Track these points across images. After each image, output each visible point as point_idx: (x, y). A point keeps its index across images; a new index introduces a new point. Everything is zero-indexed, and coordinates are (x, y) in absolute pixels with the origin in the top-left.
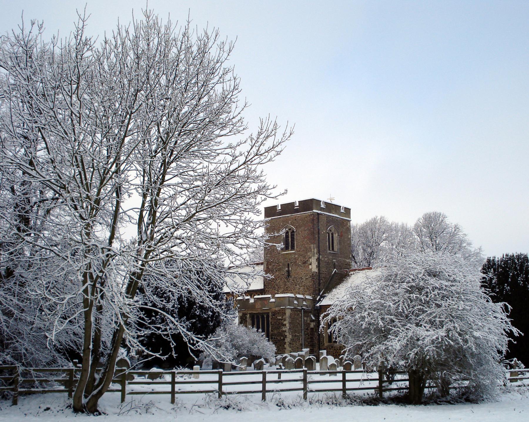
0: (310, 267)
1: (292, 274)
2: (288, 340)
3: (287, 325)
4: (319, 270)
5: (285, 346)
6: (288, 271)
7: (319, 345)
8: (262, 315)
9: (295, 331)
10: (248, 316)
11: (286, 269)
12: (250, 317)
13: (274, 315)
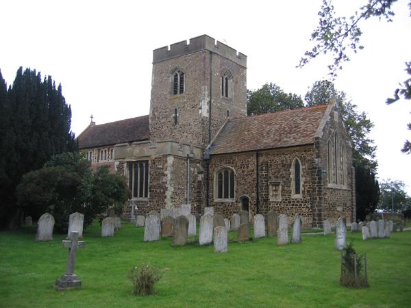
0: (200, 111)
1: (181, 121)
2: (169, 194)
3: (169, 175)
4: (210, 115)
5: (165, 200)
6: (175, 118)
7: (207, 200)
8: (141, 162)
9: (179, 184)
10: (125, 165)
11: (174, 115)
12: (127, 166)
13: (154, 163)
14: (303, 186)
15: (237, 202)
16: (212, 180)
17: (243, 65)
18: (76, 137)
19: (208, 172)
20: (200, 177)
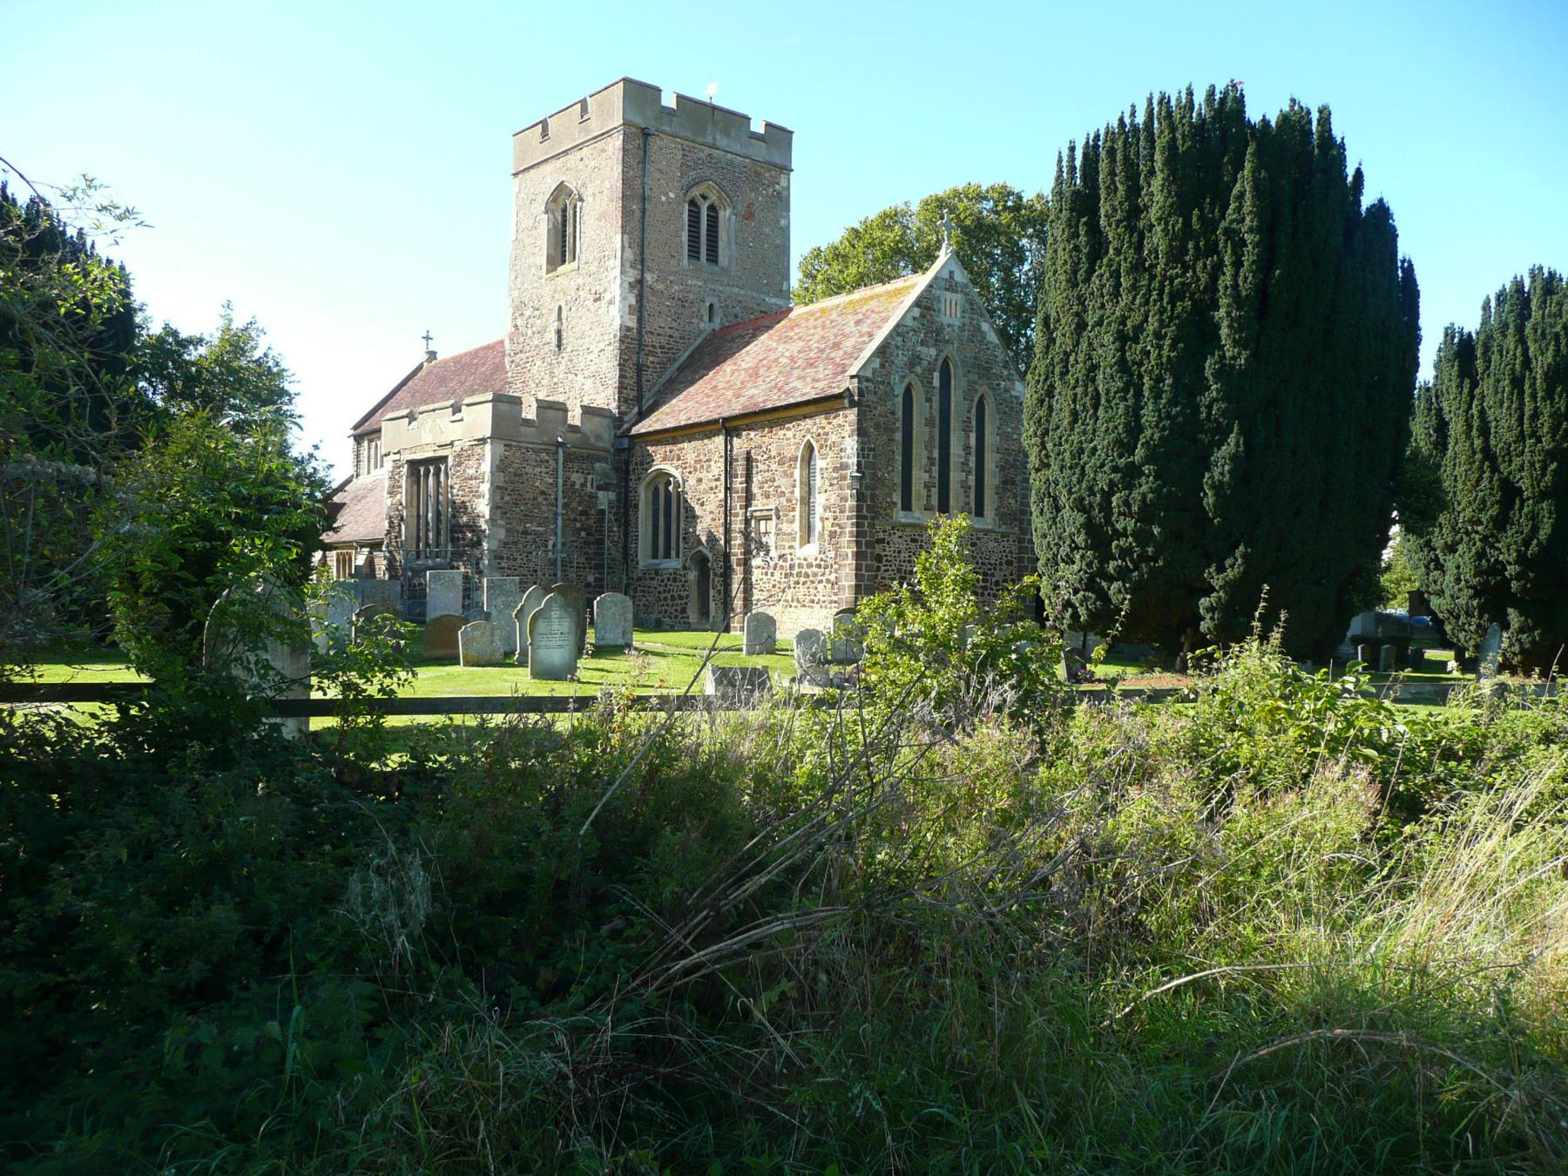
4: (640, 320)
14: (822, 519)
15: (685, 568)
16: (636, 506)
17: (777, 158)
18: (1273, 124)
19: (627, 487)
20: (605, 499)
